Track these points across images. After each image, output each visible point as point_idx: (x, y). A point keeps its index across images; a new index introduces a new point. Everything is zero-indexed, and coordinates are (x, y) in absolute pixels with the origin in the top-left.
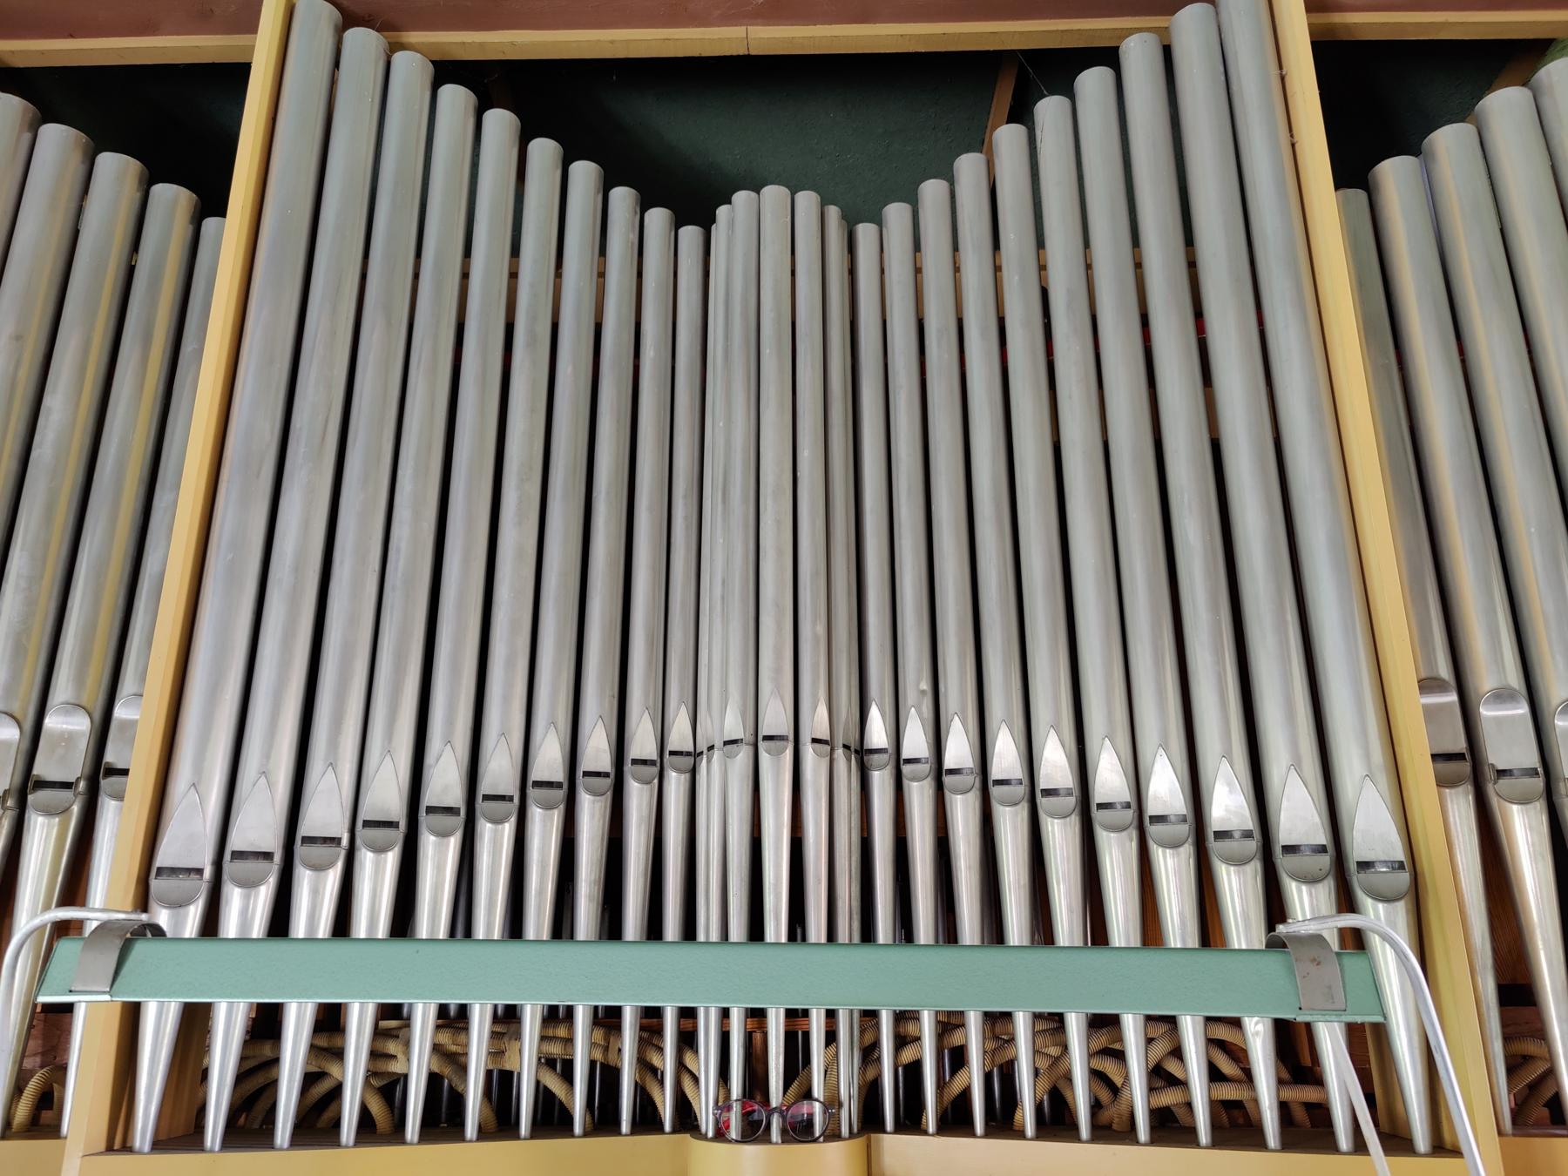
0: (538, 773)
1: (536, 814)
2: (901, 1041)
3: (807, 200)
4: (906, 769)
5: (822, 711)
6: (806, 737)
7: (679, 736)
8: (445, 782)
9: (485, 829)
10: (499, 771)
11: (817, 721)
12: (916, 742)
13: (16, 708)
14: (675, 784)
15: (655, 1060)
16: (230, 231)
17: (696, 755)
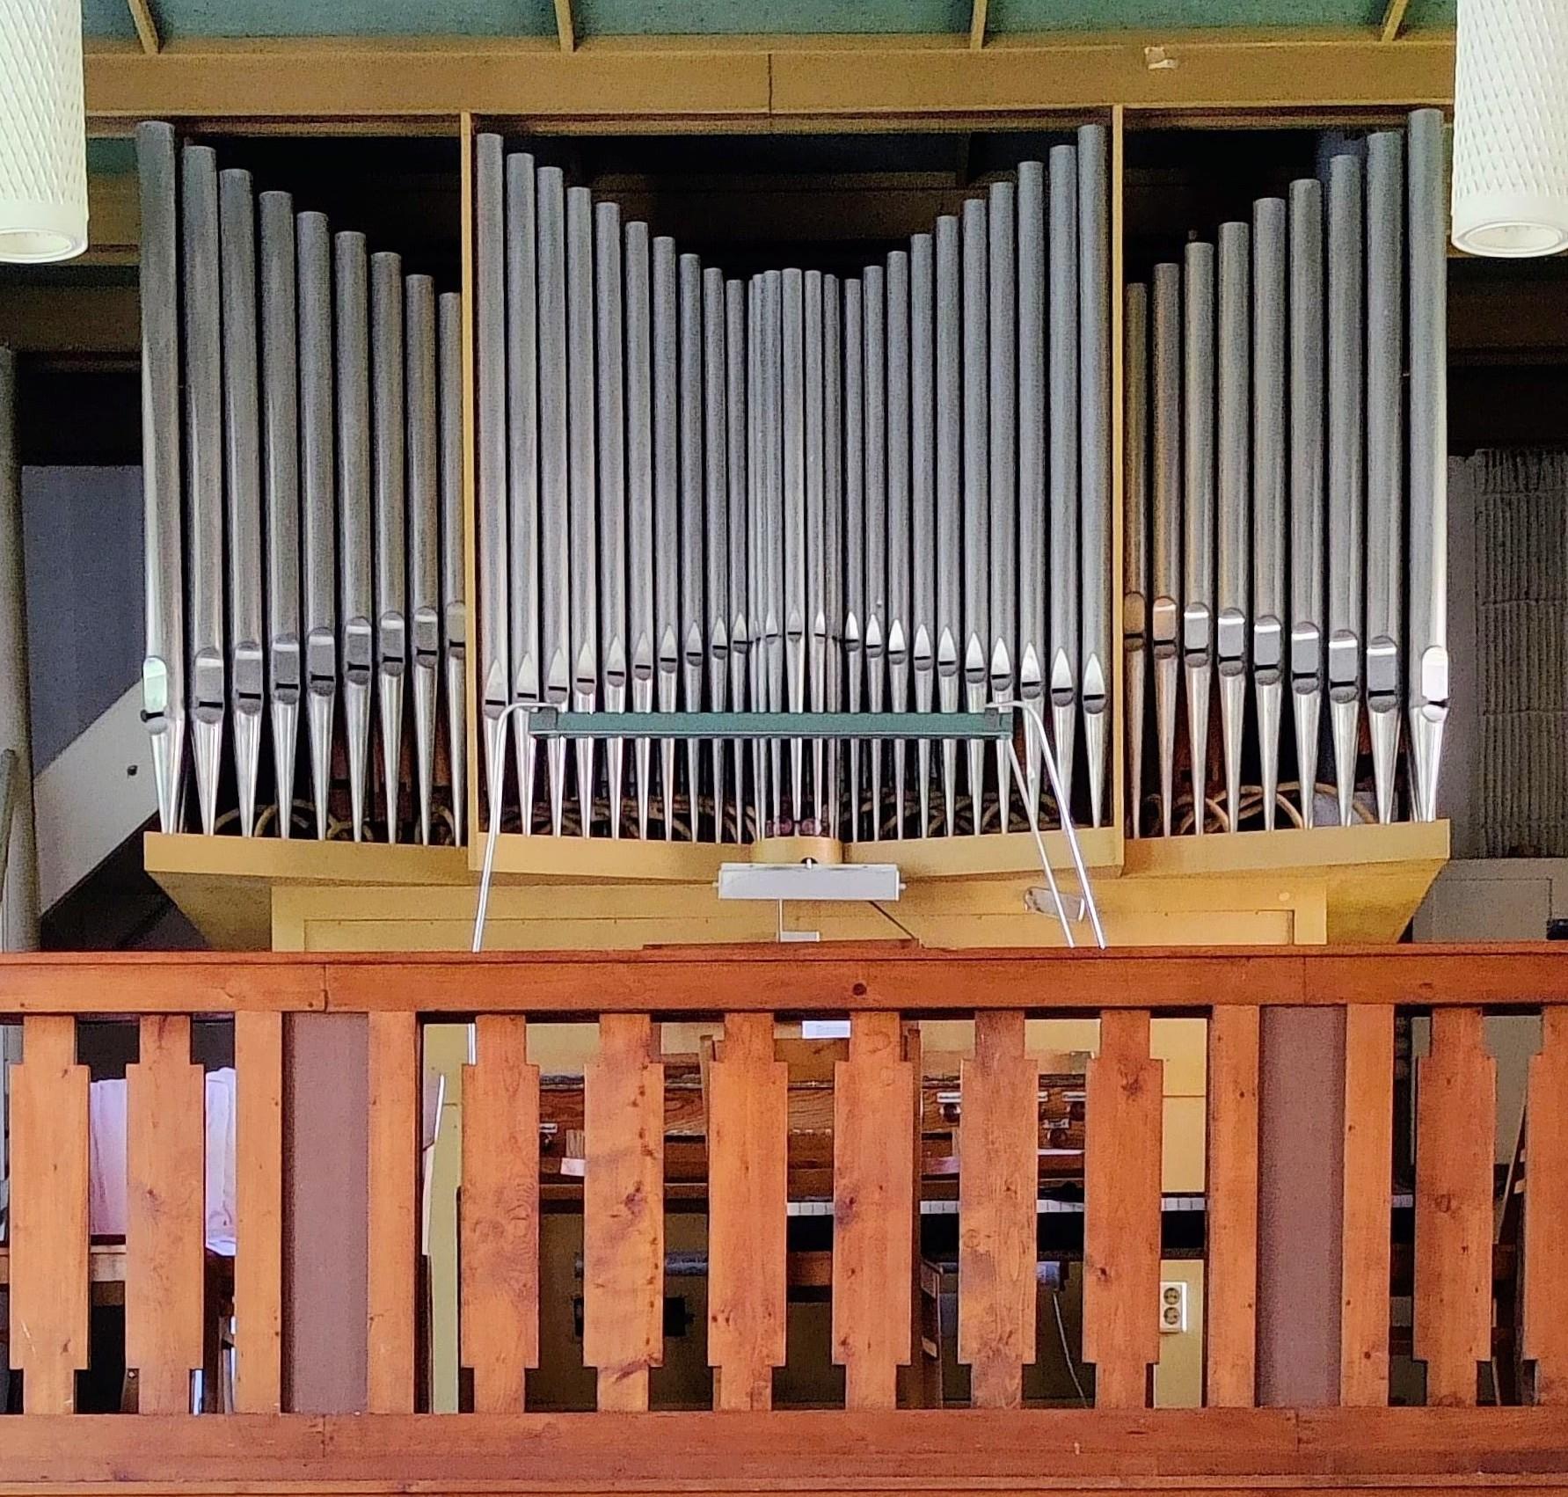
0: (663, 654)
1: (662, 674)
2: (862, 801)
3: (813, 275)
4: (869, 651)
5: (821, 617)
6: (811, 633)
7: (739, 631)
8: (615, 660)
9: (637, 682)
10: (643, 652)
11: (819, 623)
12: (874, 636)
13: (363, 614)
14: (737, 659)
15: (731, 811)
16: (458, 306)
17: (749, 643)
